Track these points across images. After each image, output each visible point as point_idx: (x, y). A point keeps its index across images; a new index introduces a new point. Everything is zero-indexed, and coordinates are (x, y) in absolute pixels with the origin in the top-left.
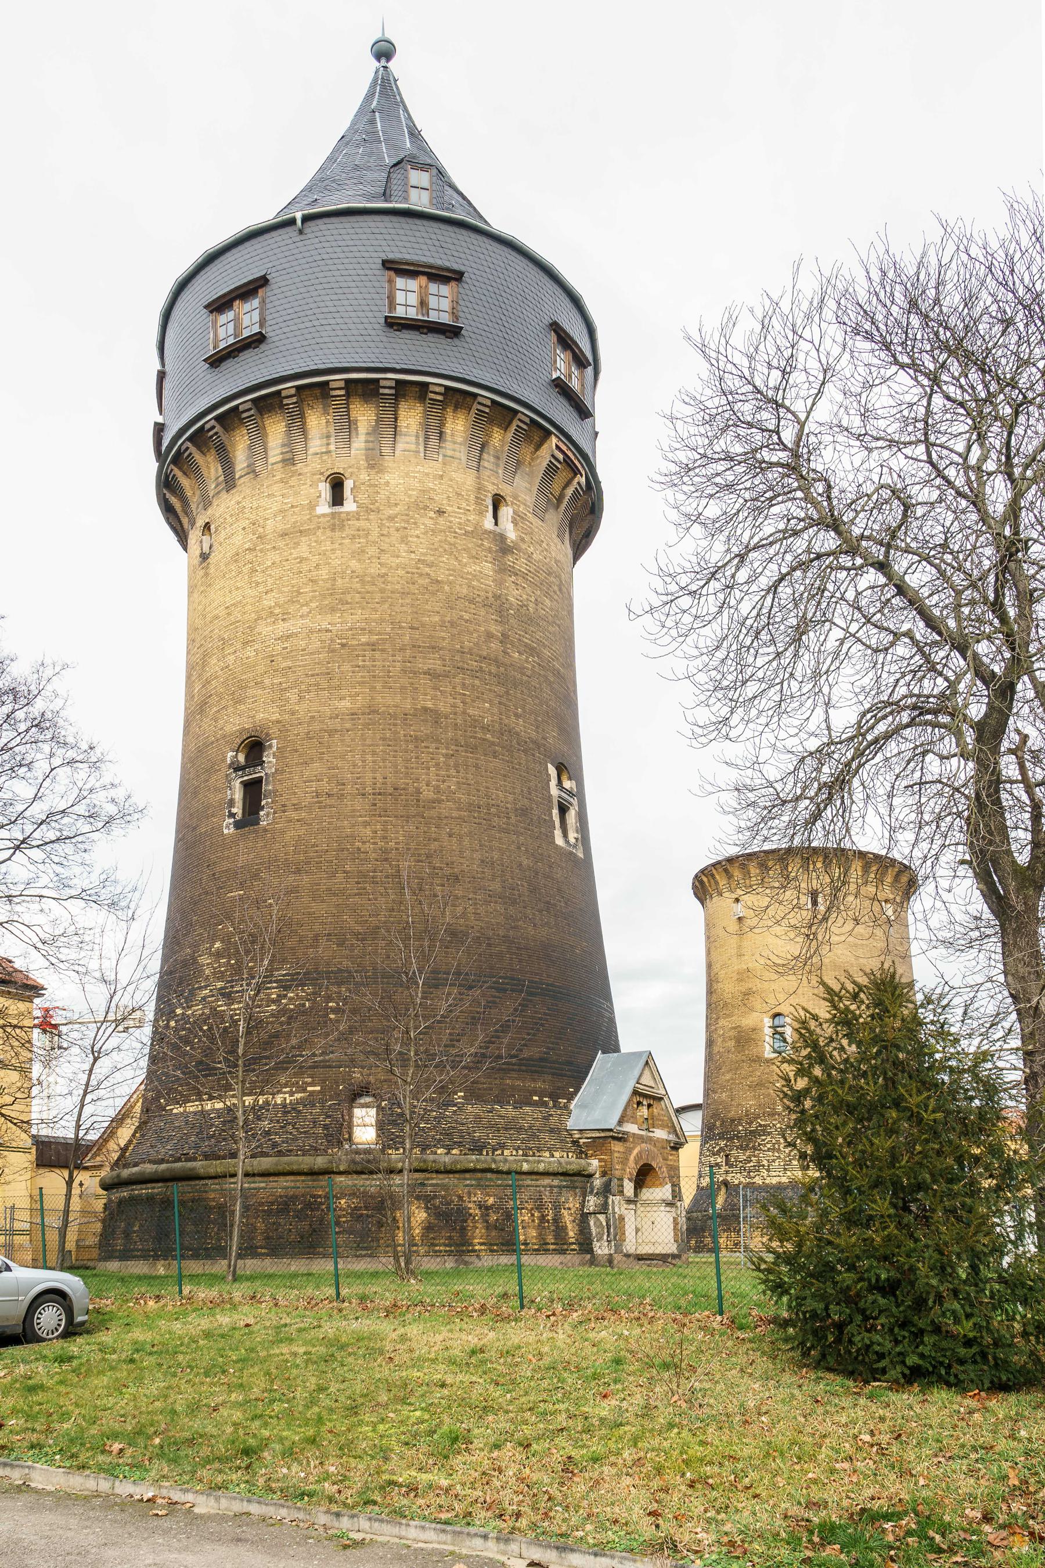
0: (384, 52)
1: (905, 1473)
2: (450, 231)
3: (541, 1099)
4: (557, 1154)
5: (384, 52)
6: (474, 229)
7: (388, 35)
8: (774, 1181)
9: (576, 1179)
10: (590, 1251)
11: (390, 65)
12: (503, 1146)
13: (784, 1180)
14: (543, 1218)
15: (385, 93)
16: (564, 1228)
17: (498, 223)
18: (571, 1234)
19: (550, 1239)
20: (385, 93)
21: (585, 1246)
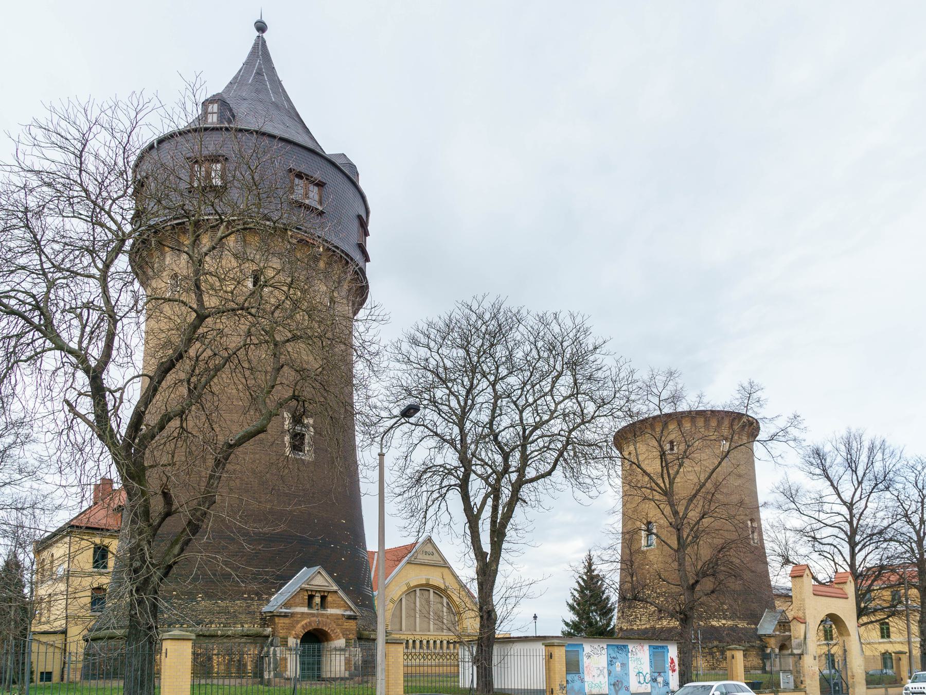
0: (261, 27)
1: (831, 627)
2: (306, 153)
3: (249, 596)
4: (246, 626)
5: (261, 27)
6: (315, 152)
7: (264, 19)
8: (644, 627)
9: (259, 639)
10: (262, 677)
11: (265, 35)
12: (211, 623)
13: (648, 626)
14: (231, 660)
15: (260, 51)
16: (245, 665)
17: (362, 184)
18: (249, 668)
19: (234, 670)
20: (260, 51)
21: (258, 673)
